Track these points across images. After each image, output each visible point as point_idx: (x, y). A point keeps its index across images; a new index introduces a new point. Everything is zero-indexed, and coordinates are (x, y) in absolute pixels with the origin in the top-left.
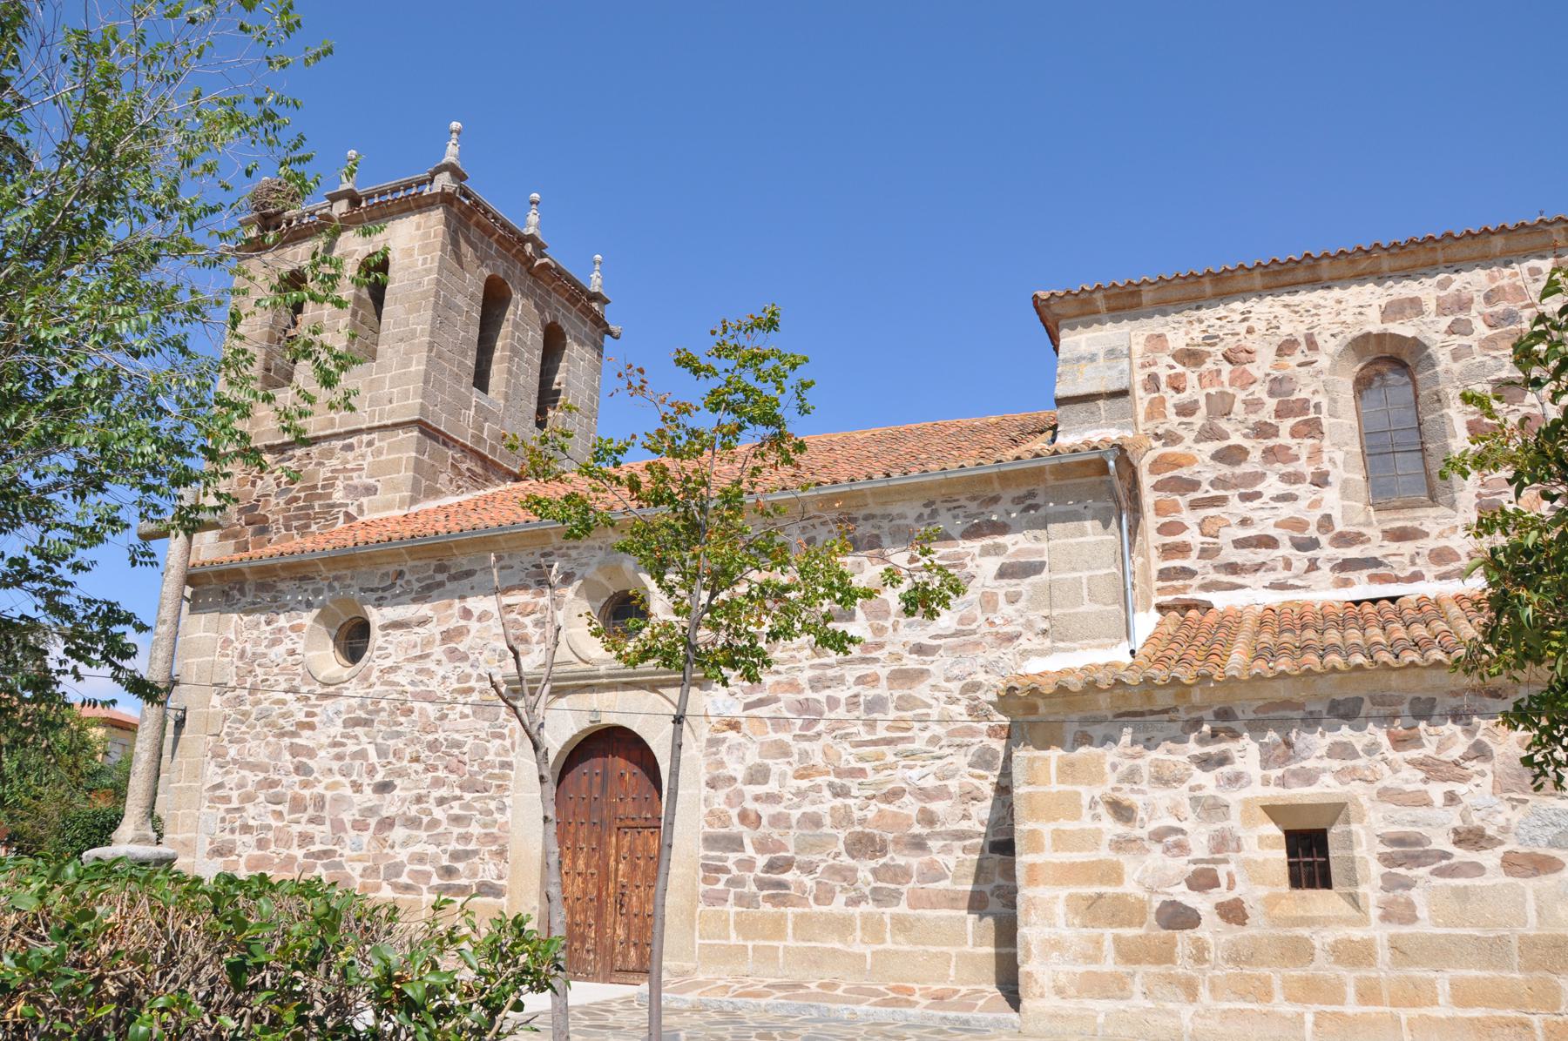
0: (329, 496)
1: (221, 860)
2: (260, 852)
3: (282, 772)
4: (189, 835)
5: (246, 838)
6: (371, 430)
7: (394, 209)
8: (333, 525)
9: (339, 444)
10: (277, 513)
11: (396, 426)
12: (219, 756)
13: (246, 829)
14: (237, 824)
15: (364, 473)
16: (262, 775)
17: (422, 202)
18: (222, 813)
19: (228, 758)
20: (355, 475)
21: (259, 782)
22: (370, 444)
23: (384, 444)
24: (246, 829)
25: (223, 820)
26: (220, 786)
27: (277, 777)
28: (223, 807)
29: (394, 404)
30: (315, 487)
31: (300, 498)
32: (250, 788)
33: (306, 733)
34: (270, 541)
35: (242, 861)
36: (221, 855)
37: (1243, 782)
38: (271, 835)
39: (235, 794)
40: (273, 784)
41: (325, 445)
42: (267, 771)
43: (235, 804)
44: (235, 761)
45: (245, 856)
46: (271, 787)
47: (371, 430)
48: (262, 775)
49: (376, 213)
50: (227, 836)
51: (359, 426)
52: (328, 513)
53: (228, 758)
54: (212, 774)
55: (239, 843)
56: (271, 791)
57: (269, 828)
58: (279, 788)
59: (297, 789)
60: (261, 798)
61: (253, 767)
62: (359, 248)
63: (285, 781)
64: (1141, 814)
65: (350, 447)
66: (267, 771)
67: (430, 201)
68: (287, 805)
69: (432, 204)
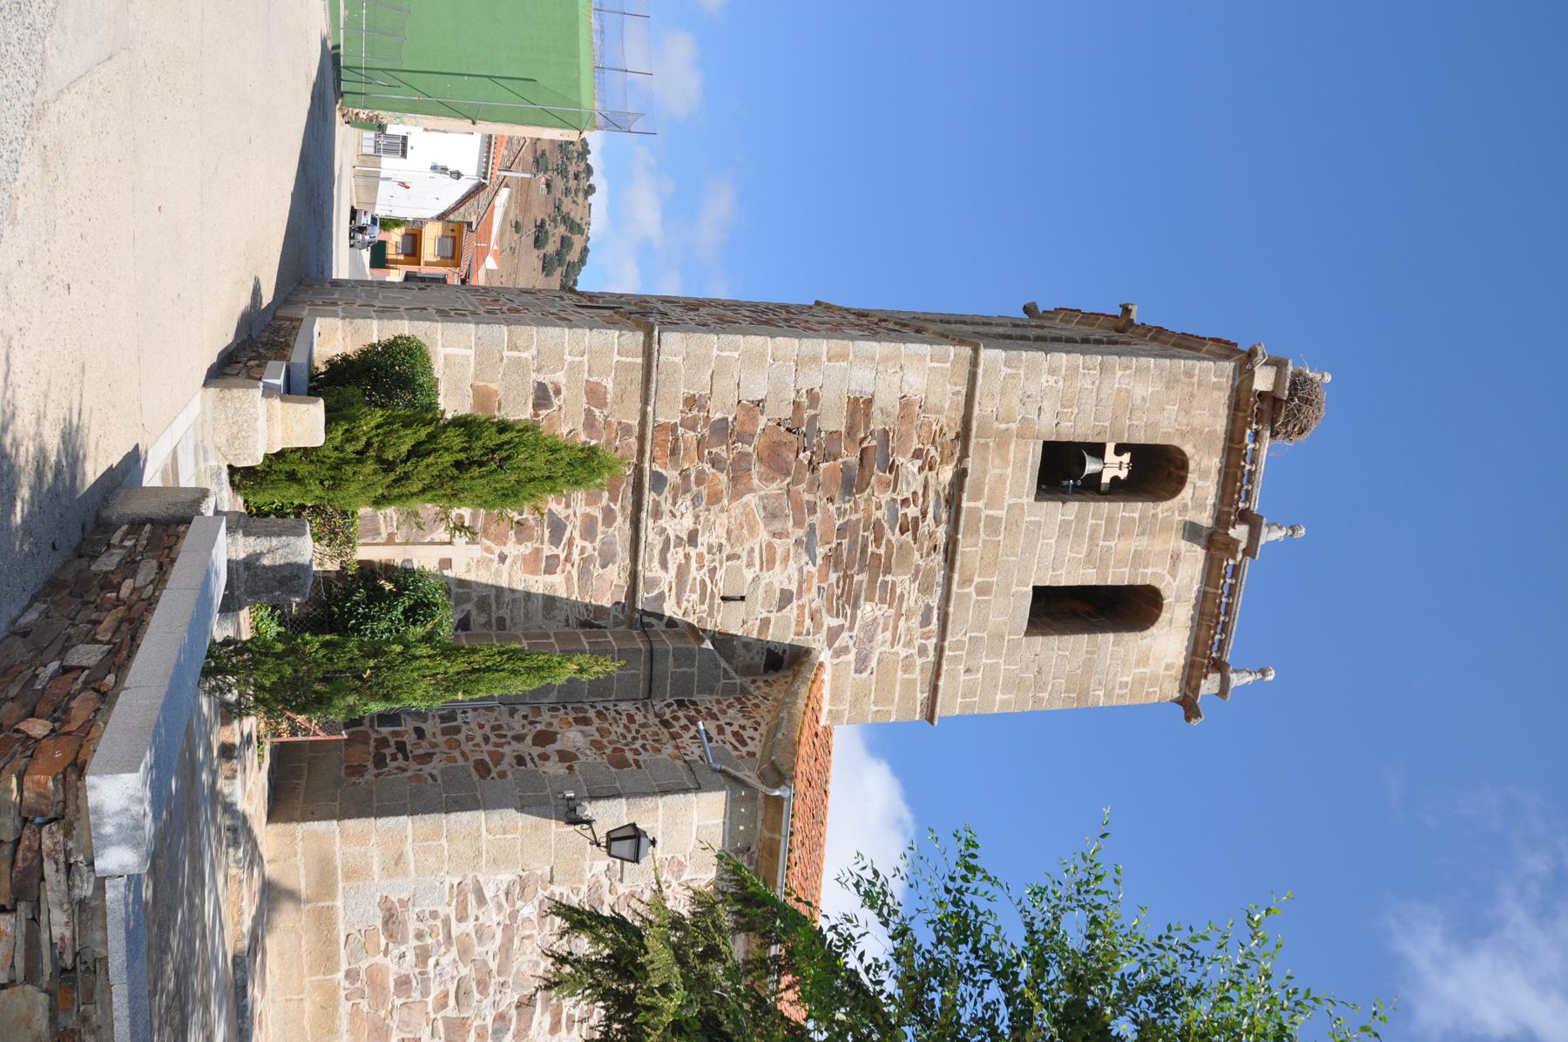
0: (870, 599)
1: (379, 923)
2: (392, 984)
3: (498, 997)
4: (412, 866)
5: (410, 958)
6: (940, 651)
7: (1203, 633)
8: (829, 611)
9: (934, 601)
10: (867, 510)
11: (934, 689)
12: (523, 889)
13: (423, 955)
14: (429, 941)
15: (886, 648)
16: (493, 966)
17: (1195, 673)
18: (443, 910)
19: (519, 904)
20: (888, 635)
21: (485, 963)
22: (922, 651)
23: (916, 674)
24: (423, 955)
25: (434, 915)
26: (481, 900)
27: (491, 990)
28: (452, 911)
29: (962, 678)
30: (888, 571)
31: (878, 547)
32: (478, 950)
33: (547, 1020)
34: (831, 500)
35: (380, 958)
36: (386, 923)
37: (516, 754)
38: (416, 995)
39: (469, 926)
40: (483, 986)
41: (939, 577)
42: (499, 973)
43: (456, 929)
44: (513, 915)
45: (387, 961)
46: (478, 984)
47: (940, 651)
48: (493, 966)
49: (1209, 606)
50: (412, 926)
51: (952, 603)
52: (848, 602)
53: (519, 904)
54: (495, 882)
55: (403, 948)
56: (474, 984)
57: (425, 993)
58: (477, 996)
59: (478, 1022)
60: (464, 971)
61: (505, 950)
62: (1176, 583)
63: (488, 1002)
64: (484, 909)
65: (926, 621)
66: (499, 973)
67: (1193, 683)
68: (455, 1014)
69: (1188, 683)
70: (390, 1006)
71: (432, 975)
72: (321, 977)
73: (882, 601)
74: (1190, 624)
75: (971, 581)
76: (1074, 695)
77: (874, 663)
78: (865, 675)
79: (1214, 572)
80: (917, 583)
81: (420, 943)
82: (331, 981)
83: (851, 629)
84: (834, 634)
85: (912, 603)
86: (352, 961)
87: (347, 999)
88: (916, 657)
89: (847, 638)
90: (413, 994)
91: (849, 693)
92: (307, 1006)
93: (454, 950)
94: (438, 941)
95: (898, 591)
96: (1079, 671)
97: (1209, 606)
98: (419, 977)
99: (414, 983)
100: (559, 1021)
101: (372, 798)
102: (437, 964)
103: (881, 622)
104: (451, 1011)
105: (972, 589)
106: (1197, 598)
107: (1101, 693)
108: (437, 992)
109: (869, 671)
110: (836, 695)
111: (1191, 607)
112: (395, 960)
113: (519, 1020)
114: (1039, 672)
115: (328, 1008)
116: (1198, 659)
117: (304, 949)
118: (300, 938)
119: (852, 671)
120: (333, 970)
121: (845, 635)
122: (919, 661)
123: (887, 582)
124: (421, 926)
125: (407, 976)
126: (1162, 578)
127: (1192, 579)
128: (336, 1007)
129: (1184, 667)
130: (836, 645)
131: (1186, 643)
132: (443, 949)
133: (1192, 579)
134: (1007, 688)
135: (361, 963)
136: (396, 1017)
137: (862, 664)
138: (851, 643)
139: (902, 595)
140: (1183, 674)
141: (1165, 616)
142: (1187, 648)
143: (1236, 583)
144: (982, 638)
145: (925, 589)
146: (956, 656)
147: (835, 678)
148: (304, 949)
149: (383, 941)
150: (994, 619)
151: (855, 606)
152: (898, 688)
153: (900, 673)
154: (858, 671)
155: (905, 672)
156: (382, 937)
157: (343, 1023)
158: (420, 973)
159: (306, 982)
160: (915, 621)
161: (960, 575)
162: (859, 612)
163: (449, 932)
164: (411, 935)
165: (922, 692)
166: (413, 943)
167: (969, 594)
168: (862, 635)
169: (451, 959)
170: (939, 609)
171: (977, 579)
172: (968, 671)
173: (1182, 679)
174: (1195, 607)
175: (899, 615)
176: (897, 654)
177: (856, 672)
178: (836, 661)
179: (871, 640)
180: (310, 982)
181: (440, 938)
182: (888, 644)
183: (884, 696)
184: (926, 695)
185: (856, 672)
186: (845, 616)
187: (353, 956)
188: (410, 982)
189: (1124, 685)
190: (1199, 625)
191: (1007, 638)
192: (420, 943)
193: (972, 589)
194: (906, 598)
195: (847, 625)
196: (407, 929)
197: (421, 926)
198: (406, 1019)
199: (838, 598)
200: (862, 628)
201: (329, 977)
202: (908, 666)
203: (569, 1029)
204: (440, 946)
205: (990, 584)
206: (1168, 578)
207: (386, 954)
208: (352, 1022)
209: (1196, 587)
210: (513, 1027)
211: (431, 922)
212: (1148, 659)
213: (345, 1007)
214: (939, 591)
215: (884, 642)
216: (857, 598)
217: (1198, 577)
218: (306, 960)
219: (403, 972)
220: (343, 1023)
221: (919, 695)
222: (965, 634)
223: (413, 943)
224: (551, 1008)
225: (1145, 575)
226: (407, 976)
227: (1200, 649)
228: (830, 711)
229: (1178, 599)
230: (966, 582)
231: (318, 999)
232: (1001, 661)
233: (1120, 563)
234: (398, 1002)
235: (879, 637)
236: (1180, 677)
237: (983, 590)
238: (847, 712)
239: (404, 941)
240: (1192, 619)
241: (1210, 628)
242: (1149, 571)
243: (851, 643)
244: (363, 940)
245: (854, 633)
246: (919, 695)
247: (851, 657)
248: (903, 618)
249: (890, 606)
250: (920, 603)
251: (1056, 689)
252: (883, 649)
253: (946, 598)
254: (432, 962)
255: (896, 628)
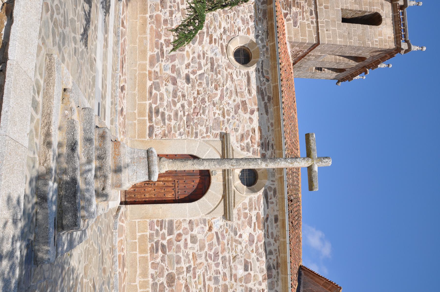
0: (294, 6)
2: (162, 21)
5: (168, 14)
6: (317, 22)
7: (397, 27)
8: (283, 8)
9: (313, 9)
11: (318, 34)
13: (171, 13)
14: (173, 9)
17: (398, 39)
20: (301, 16)
22: (312, 22)
23: (312, 29)
24: (171, 13)
29: (326, 32)
43: (181, 7)
45: (161, 14)
47: (317, 22)
52: (288, 6)
55: (166, 10)
62: (384, 12)
65: (311, 14)
67: (398, 42)
69: (397, 43)
70: (162, 28)
71: (174, 20)
72: (142, 15)
73: (298, 7)
74: (392, 25)
75: (322, 5)
76: (361, 42)
77: (299, 24)
78: (297, 27)
79: (395, 9)
80: (307, 3)
81: (170, 9)
82: (145, 17)
83: (290, 14)
84: (286, 15)
85: (306, 9)
86: (151, 12)
87: (149, 24)
88: (311, 24)
89: (289, 16)
90: (168, 25)
91: (293, 32)
92: (138, 23)
93: (180, 13)
94: (176, 9)
95: (302, 5)
96: (361, 35)
97: (397, 19)
98: (170, 20)
99: (169, 21)
100: (212, 40)
101: (149, 236)
102: (175, 17)
103: (299, 13)
104: (176, 100)
105: (323, 7)
106: (392, 17)
107: (370, 43)
108: (175, 25)
109: (298, 27)
110: (289, 32)
111: (391, 20)
112: (163, 14)
113: (200, 38)
114: (349, 33)
115: (144, 25)
116: (398, 35)
117: (138, 6)
118: (137, 3)
119: (293, 26)
120: (146, 13)
121: (289, 15)
122: (312, 25)
123: (298, 2)
124: (171, 4)
125: (167, 19)
126: (380, 10)
127: (389, 12)
128: (146, 25)
129: (394, 38)
130: (287, 18)
131: (393, 31)
132: (177, 12)
133: (389, 12)
134: (340, 37)
135: (154, 13)
136: (163, 31)
137: (295, 24)
138: (291, 18)
139: (303, 6)
140: (394, 40)
141: (383, 22)
142: (393, 32)
143: (404, 17)
144: (329, 21)
145: (309, 5)
146: (322, 26)
147: (288, 27)
148: (138, 6)
149: (160, 8)
150: (331, 16)
151: (290, 8)
152: (307, 32)
153: (307, 28)
154: (295, 26)
155: (308, 28)
156: (160, 7)
157: (148, 31)
158: (171, 19)
159: (138, 16)
160: (308, 14)
161: (319, 3)
162: (292, 10)
163: (179, 7)
164: (168, 6)
165: (315, 35)
166: (168, 9)
167: (322, 8)
168: (294, 16)
169: (179, 16)
170: (314, 11)
171: (324, 5)
172: (327, 30)
173: (395, 42)
174: (392, 20)
175: (303, 12)
176: (305, 22)
177: (294, 26)
178: (287, 22)
179: (296, 17)
180: (140, 16)
181: (176, 8)
182: (302, 19)
183: (303, 34)
184: (316, 35)
185: (294, 26)
186: (288, 10)
187: (152, 11)
188: (168, 21)
189: (376, 41)
190: (395, 25)
191: (336, 22)
192: (170, 9)
193: (323, 7)
194: (304, 7)
195: (289, 13)
196: (167, 5)
197: (171, 4)
198: (166, 33)
199: (285, 5)
200: (293, 14)
201: (144, 15)
202: (309, 27)
203: (215, 43)
204: (176, 11)
205: (328, 6)
206: (381, 11)
207: (161, 12)
208: (151, 31)
209: (391, 14)
210: (198, 40)
211: (174, 4)
212: (382, 34)
213: (149, 26)
214: (314, 6)
215: (300, 19)
216: (290, 6)
217: (391, 11)
218: (139, 9)
219: (166, 18)
220: (148, 31)
221: (314, 35)
222: (324, 19)
223: (168, 9)
224: (209, 36)
225: (374, 9)
226: (167, 19)
227: (398, 32)
228: (288, 37)
229: (386, 17)
230: (321, 5)
231: (141, 21)
232: (337, 29)
233: (365, 4)
234: (164, 27)
235: (299, 17)
236: (394, 41)
237: (326, 7)
238: (293, 38)
239: (166, 8)
240: (393, 23)
241: (399, 25)
242: (375, 8)
243: (291, 18)
244: (154, 6)
245: (291, 15)
246: (314, 35)
247: (292, 22)
248: (305, 13)
249: (300, 9)
250: (309, 9)
251: (355, 39)
252: (300, 21)
253: (316, 8)
254: (174, 16)
255: (303, 15)
